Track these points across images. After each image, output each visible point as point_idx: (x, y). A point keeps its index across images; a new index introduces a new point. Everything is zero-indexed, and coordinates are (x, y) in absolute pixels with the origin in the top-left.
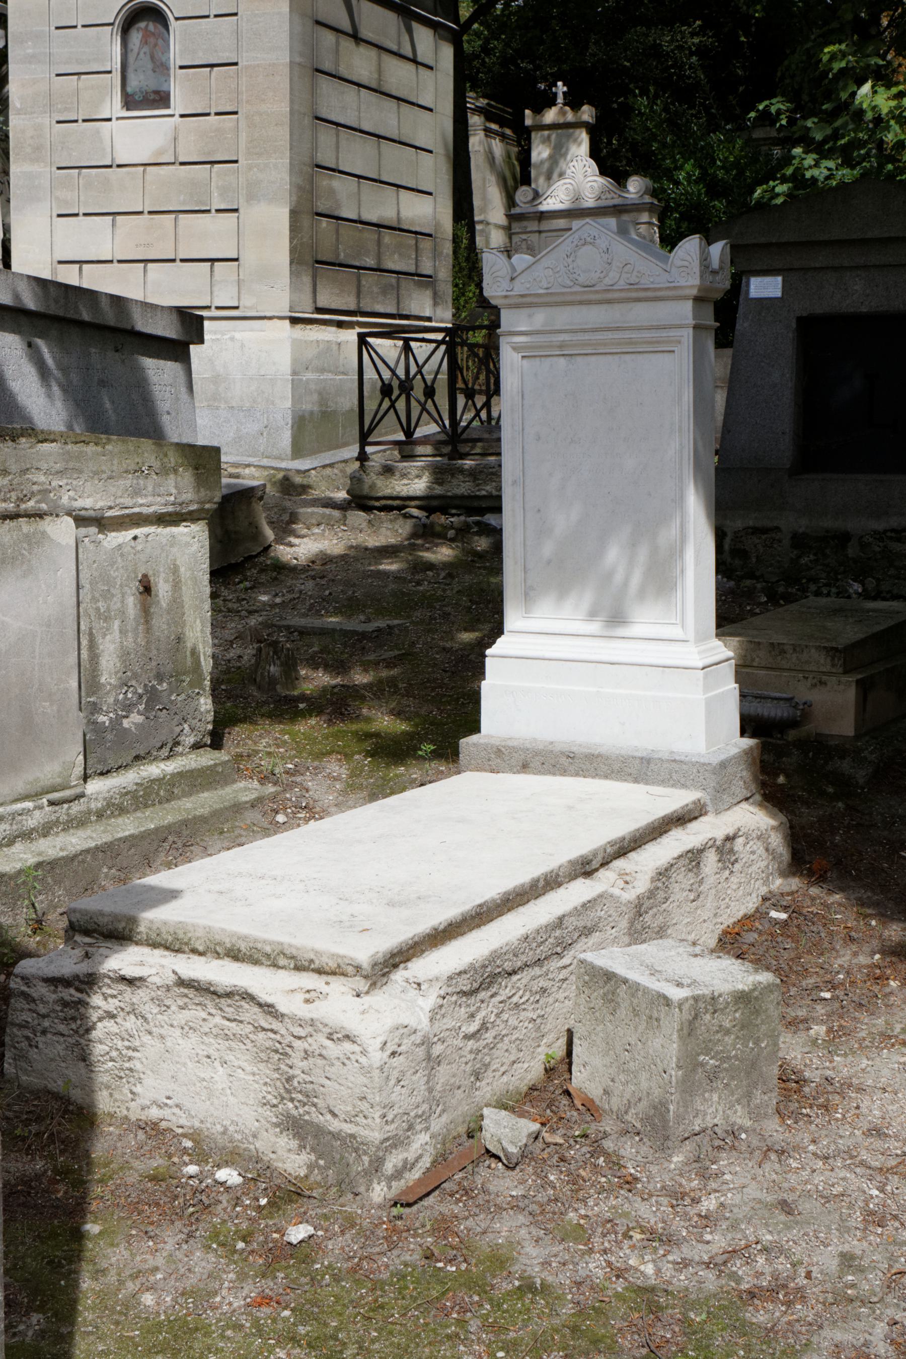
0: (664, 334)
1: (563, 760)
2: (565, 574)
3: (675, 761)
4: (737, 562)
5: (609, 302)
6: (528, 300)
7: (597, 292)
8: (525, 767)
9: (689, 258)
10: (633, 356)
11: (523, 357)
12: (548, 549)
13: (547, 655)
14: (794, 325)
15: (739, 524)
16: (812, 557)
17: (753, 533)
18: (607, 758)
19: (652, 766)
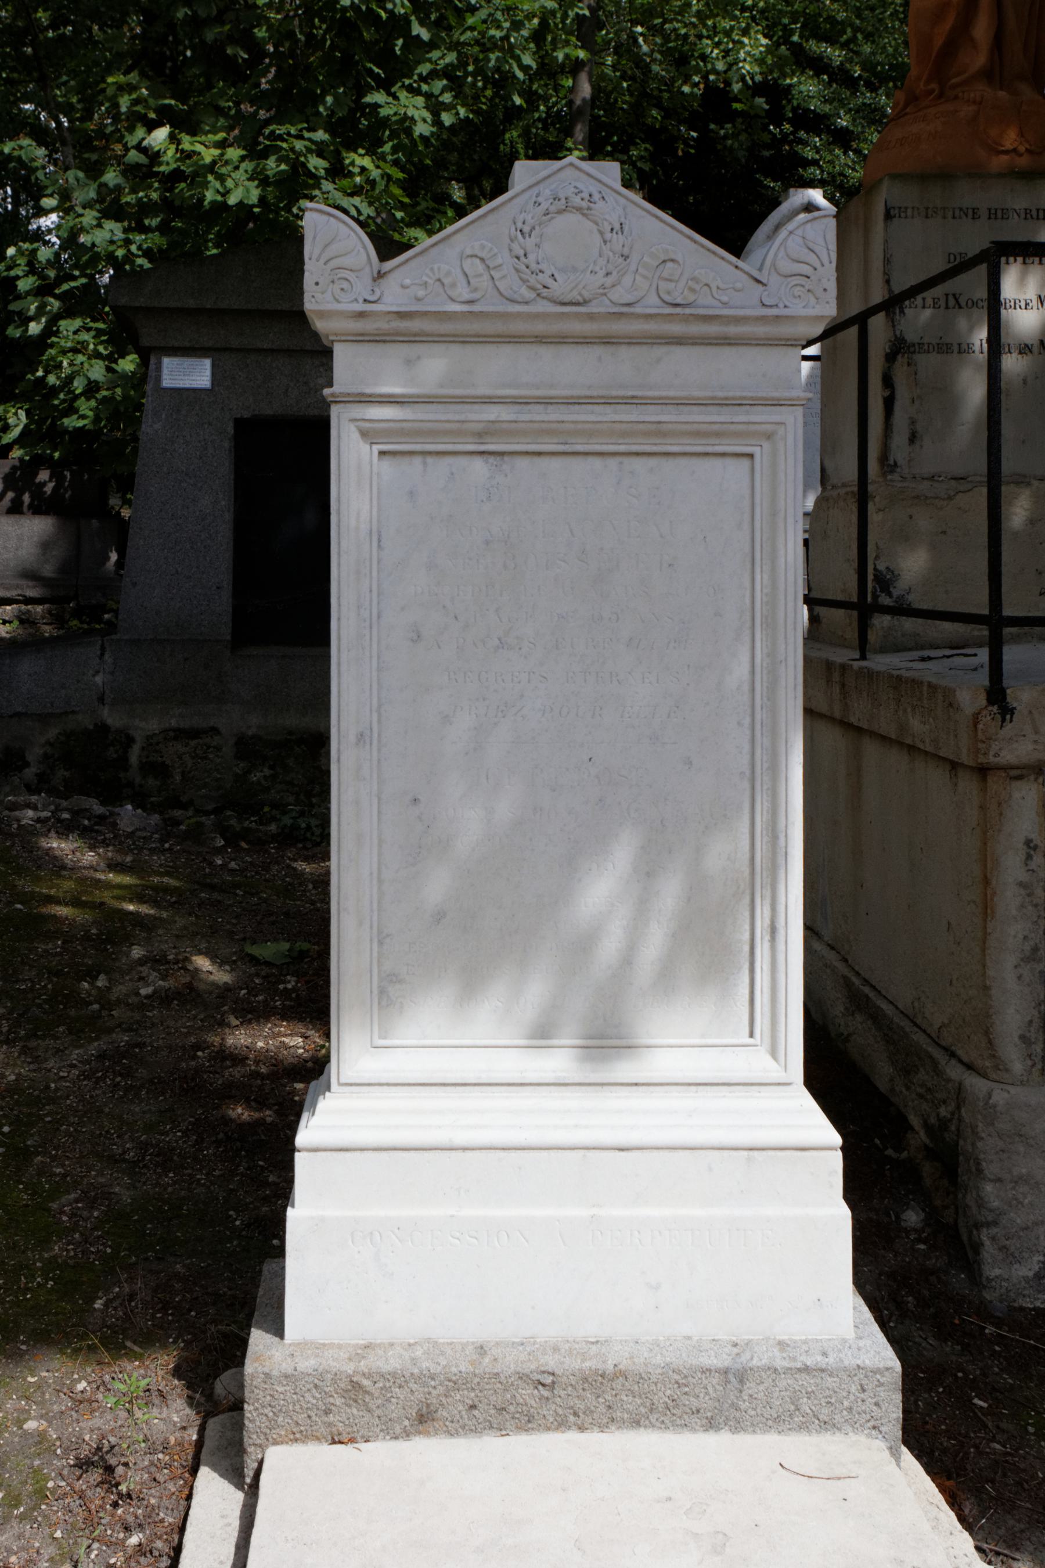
0: (741, 416)
1: (526, 1393)
2: (479, 942)
3: (806, 1369)
4: (151, 782)
5: (607, 341)
6: (415, 325)
7: (591, 317)
8: (424, 1420)
9: (812, 258)
10: (652, 462)
11: (382, 453)
12: (437, 886)
13: (461, 1138)
14: (230, 429)
15: (153, 725)
16: (267, 772)
17: (176, 738)
18: (640, 1378)
19: (750, 1387)
